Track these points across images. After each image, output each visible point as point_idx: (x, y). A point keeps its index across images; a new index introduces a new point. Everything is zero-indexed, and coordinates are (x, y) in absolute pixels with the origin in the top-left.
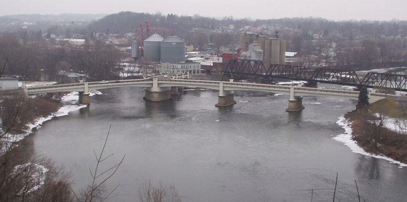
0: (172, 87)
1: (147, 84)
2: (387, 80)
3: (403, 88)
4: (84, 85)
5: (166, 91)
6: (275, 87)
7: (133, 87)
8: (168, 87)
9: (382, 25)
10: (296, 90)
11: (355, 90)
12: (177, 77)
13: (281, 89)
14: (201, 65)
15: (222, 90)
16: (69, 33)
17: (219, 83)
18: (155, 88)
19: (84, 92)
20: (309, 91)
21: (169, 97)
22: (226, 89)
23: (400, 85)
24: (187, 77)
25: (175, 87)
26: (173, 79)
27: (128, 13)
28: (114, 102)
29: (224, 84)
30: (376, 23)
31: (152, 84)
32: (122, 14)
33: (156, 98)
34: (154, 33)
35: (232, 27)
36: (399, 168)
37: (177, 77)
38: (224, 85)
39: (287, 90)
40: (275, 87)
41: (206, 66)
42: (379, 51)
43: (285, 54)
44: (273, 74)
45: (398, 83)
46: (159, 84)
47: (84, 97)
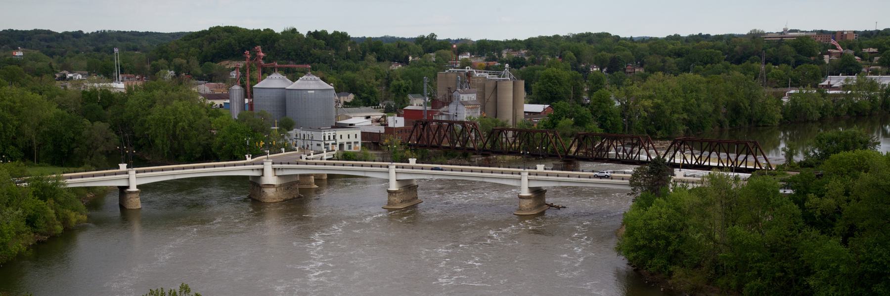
0: (301, 175)
2: (747, 154)
3: (743, 166)
4: (127, 173)
8: (297, 175)
12: (312, 156)
13: (504, 175)
15: (395, 180)
17: (387, 167)
19: (128, 187)
21: (296, 193)
23: (736, 160)
25: (309, 175)
26: (304, 160)
27: (229, 30)
28: (406, 186)
32: (245, 29)
34: (418, 93)
36: (792, 189)
37: (312, 156)
42: (630, 53)
44: (456, 146)
47: (676, 162)
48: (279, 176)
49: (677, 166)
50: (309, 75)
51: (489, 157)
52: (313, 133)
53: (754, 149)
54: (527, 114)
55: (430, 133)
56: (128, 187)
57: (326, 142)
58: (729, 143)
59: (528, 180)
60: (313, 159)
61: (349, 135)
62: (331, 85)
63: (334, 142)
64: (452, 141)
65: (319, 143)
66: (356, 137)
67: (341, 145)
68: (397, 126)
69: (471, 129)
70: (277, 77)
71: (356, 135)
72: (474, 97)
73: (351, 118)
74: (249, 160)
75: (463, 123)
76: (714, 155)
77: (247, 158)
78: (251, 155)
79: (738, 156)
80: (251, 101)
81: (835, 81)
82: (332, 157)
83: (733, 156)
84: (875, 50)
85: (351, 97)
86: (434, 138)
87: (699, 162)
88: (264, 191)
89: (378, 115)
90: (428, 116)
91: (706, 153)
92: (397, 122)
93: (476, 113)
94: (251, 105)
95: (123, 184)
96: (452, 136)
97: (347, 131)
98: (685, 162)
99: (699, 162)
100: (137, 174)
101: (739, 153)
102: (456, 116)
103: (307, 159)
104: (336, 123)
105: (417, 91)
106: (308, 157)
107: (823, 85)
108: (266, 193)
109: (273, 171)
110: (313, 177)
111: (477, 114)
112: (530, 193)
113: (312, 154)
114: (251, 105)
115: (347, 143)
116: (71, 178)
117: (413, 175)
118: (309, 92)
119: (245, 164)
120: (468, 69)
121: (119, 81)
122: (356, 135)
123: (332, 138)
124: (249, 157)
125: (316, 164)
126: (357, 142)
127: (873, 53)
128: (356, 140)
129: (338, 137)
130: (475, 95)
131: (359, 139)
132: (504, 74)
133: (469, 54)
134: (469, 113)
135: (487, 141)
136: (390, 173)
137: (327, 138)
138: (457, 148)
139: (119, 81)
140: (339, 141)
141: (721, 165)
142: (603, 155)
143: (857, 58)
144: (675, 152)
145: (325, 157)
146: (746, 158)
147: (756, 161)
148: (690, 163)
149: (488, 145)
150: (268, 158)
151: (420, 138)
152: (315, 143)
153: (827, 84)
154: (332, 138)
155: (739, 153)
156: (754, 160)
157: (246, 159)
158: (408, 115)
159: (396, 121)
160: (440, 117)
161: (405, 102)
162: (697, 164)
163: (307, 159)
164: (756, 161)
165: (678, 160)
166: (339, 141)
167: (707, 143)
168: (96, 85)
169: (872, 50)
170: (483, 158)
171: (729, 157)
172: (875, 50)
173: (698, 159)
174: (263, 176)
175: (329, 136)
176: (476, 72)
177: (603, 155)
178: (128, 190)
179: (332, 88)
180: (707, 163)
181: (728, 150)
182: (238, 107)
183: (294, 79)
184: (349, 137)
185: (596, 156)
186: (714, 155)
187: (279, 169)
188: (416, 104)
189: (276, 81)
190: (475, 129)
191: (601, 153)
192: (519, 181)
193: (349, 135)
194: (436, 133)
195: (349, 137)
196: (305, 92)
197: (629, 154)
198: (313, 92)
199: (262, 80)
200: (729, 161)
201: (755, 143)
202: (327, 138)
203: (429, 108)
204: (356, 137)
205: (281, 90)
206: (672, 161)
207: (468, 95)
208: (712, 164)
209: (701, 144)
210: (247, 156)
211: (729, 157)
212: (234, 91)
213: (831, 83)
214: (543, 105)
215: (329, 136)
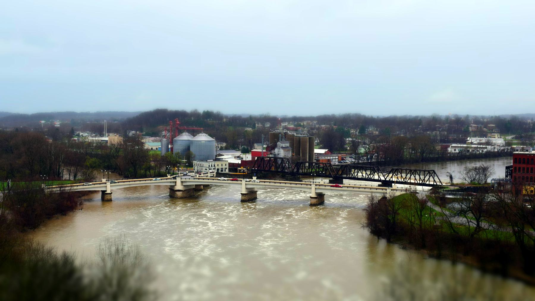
0: (196, 185)
1: (171, 182)
4: (106, 183)
5: (135, 176)
6: (302, 184)
7: (146, 186)
8: (193, 185)
9: (420, 120)
10: (317, 187)
11: (379, 185)
12: (202, 175)
14: (229, 163)
16: (99, 130)
17: (241, 181)
18: (179, 187)
19: (106, 191)
20: (128, 183)
22: (249, 187)
23: (406, 177)
24: (214, 175)
26: (197, 177)
29: (246, 181)
30: (417, 117)
31: (106, 187)
33: (156, 174)
35: (268, 125)
38: (246, 182)
39: (309, 186)
40: (302, 184)
41: (233, 164)
43: (313, 151)
45: (422, 177)
46: (182, 182)
48: (184, 185)
49: (393, 182)
50: (202, 133)
51: (295, 177)
52: (203, 163)
53: (433, 174)
54: (316, 154)
55: (265, 164)
56: (106, 191)
57: (210, 168)
58: (420, 171)
59: (246, 184)
60: (202, 177)
61: (222, 164)
62: (214, 139)
63: (214, 168)
64: (276, 167)
65: (206, 168)
66: (226, 165)
67: (218, 170)
68: (247, 160)
69: (286, 162)
70: (204, 135)
71: (226, 164)
72: (288, 145)
73: (223, 155)
74: (169, 177)
75: (282, 159)
76: (412, 177)
77: (168, 176)
78: (170, 175)
79: (406, 175)
80: (172, 146)
81: (475, 141)
82: (213, 175)
83: (404, 175)
84: (494, 125)
85: (224, 145)
86: (267, 166)
87: (424, 182)
88: (176, 193)
89: (238, 154)
90: (264, 155)
91: (409, 175)
92: (248, 157)
93: (289, 153)
94: (172, 148)
95: (104, 189)
96: (276, 165)
97: (221, 162)
98: (398, 181)
99: (424, 182)
100: (111, 184)
101: (407, 173)
102: (279, 155)
103: (199, 176)
104: (216, 158)
105: (259, 141)
106: (200, 176)
107: (469, 142)
108: (177, 194)
109: (181, 183)
110: (202, 186)
111: (289, 155)
112: (316, 195)
113: (202, 174)
114: (172, 148)
115: (221, 168)
116: (77, 186)
117: (322, 190)
118: (202, 142)
119: (167, 179)
120: (285, 130)
121: (106, 136)
122: (226, 164)
123: (213, 166)
124: (169, 175)
125: (204, 179)
126: (226, 168)
127: (493, 127)
128: (226, 167)
129: (216, 165)
130: (289, 144)
131: (227, 166)
132: (304, 134)
133: (287, 123)
134: (285, 153)
135: (294, 168)
136: (312, 188)
137: (210, 166)
138: (279, 172)
139: (106, 136)
140: (217, 167)
141: (416, 182)
142: (355, 176)
143: (485, 129)
144: (430, 177)
145: (209, 176)
146: (429, 179)
147: (434, 181)
148: (400, 181)
149: (295, 170)
150: (178, 176)
151: (259, 166)
152: (204, 168)
153: (471, 142)
154: (213, 166)
155: (407, 173)
156: (433, 180)
157: (167, 177)
158: (254, 154)
159: (247, 157)
160: (270, 155)
161: (252, 147)
162: (404, 181)
163: (199, 176)
164: (434, 181)
165: (394, 179)
166: (217, 167)
167: (409, 171)
168: (94, 138)
169: (492, 125)
170: (292, 177)
171: (402, 176)
172: (494, 125)
173: (405, 178)
174: (176, 185)
175: (212, 165)
176: (290, 132)
177: (355, 176)
178: (106, 192)
179: (215, 140)
180: (409, 181)
181: (401, 172)
182: (165, 150)
183: (194, 136)
184: (222, 166)
185: (351, 176)
186: (412, 177)
187: (184, 182)
188: (258, 149)
189: (185, 137)
190: (288, 162)
191: (370, 176)
192: (310, 189)
193: (222, 164)
194: (268, 164)
195: (222, 166)
196: (200, 142)
197: (308, 170)
198: (204, 142)
199: (178, 136)
200: (305, 169)
201: (434, 171)
202: (210, 166)
203: (264, 151)
204: (226, 165)
205: (187, 141)
206: (391, 180)
207: (285, 144)
208: (430, 183)
209: (425, 172)
210: (168, 175)
211: (402, 176)
212: (164, 141)
213: (472, 142)
214: (325, 150)
215: (212, 165)
